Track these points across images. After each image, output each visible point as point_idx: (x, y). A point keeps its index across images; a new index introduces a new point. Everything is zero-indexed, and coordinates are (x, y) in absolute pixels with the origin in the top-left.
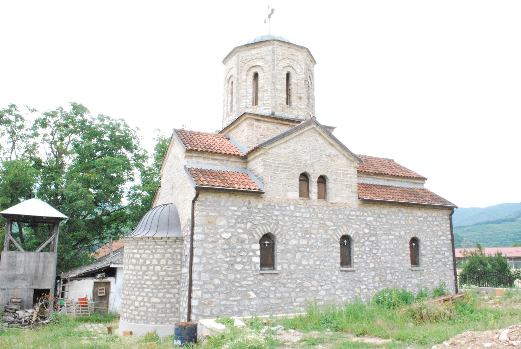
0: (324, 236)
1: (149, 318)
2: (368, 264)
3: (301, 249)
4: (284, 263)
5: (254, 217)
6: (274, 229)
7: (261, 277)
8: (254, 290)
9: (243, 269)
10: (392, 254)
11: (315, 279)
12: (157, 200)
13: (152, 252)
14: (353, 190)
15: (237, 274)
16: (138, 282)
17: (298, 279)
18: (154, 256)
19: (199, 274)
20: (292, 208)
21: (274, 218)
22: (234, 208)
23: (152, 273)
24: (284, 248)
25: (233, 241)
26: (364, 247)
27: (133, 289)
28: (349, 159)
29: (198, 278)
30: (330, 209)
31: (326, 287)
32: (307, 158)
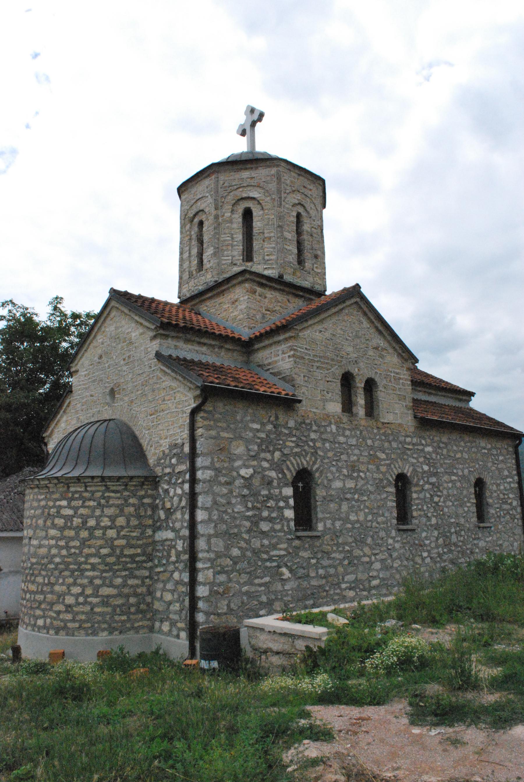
0: (376, 475)
1: (96, 625)
2: (429, 519)
3: (349, 496)
4: (327, 518)
5: (284, 442)
6: (311, 463)
7: (297, 543)
8: (289, 564)
9: (273, 530)
10: (455, 503)
11: (367, 545)
12: (62, 417)
13: (99, 504)
14: (407, 403)
15: (264, 539)
16: (70, 560)
17: (346, 544)
18: (103, 511)
19: (208, 540)
20: (334, 427)
21: (311, 444)
22: (256, 426)
23: (100, 542)
24: (325, 494)
25: (256, 482)
26: (423, 493)
27: (60, 573)
28: (402, 356)
29: (207, 548)
30: (381, 432)
31: (380, 557)
32: (350, 349)
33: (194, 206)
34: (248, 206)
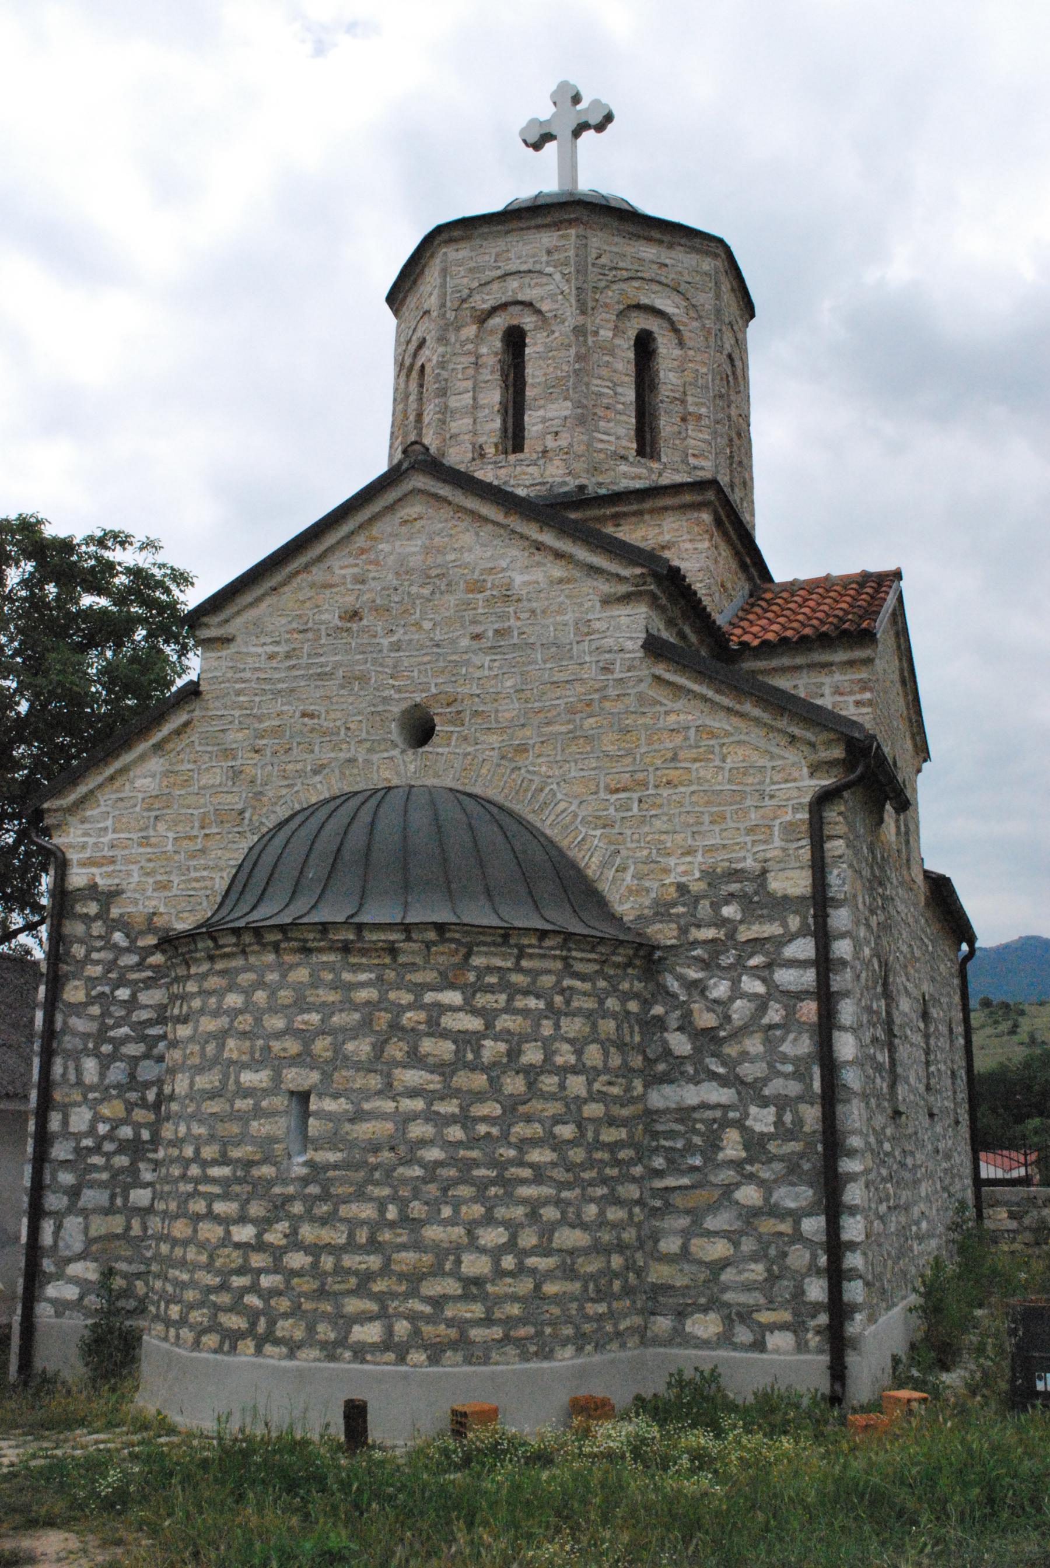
1: (548, 1330)
16: (475, 1154)
18: (557, 1026)
23: (554, 1108)
27: (445, 1190)
33: (495, 286)
34: (647, 327)
